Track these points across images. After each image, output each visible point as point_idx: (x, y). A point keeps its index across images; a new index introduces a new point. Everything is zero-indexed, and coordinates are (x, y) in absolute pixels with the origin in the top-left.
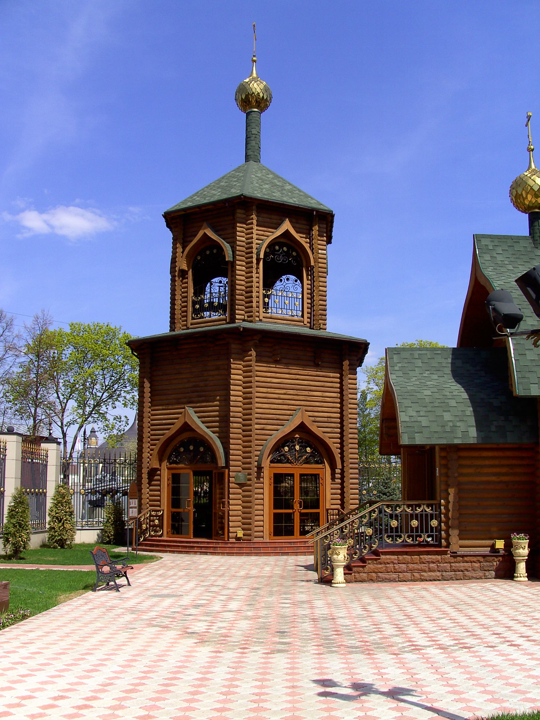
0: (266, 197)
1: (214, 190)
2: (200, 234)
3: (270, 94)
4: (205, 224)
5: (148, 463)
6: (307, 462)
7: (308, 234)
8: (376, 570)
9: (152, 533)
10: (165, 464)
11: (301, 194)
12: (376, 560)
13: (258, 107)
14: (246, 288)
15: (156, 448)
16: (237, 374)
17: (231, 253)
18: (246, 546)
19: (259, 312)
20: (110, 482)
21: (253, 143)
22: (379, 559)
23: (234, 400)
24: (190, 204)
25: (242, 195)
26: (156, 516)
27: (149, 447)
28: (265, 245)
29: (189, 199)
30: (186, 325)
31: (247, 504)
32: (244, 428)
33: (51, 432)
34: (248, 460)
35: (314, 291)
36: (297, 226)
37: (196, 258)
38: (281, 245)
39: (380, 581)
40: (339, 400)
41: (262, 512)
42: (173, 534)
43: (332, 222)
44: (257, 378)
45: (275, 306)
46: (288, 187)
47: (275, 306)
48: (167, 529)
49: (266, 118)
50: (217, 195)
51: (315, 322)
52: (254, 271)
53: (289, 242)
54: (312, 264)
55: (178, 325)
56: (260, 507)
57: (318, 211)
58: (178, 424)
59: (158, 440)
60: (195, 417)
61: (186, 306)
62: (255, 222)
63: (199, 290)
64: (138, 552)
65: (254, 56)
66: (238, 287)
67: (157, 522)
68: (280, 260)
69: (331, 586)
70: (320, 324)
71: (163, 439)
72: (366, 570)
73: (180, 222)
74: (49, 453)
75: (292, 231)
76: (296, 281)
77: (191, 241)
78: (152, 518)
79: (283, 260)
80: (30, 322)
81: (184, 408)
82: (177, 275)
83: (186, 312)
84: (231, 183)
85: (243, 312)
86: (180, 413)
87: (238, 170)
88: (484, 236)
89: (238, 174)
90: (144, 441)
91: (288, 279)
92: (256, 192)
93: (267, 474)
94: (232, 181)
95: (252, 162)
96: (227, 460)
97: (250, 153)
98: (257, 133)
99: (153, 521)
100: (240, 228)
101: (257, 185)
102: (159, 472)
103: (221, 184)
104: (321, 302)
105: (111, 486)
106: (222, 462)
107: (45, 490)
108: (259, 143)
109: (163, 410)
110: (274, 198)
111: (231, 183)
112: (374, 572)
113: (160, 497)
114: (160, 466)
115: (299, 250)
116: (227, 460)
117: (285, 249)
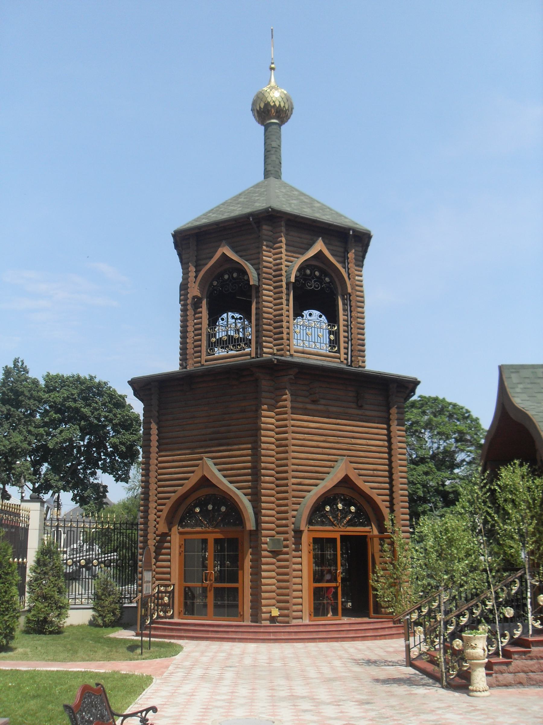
0: (296, 211)
1: (232, 206)
3: (291, 103)
4: (224, 242)
5: (155, 527)
6: (351, 523)
8: (525, 669)
9: (161, 614)
10: (175, 529)
11: (333, 212)
12: (525, 653)
13: (278, 117)
14: (275, 316)
15: (166, 509)
16: (268, 419)
17: (257, 276)
18: (279, 629)
19: (289, 346)
20: (87, 552)
21: (274, 157)
22: (530, 652)
23: (266, 447)
25: (270, 207)
26: (166, 592)
27: (156, 508)
28: (296, 267)
29: (204, 217)
30: (200, 362)
31: (283, 577)
32: (278, 482)
33: (24, 495)
34: (284, 522)
35: (351, 322)
36: (331, 248)
37: (211, 284)
39: (533, 685)
41: (299, 587)
42: (185, 614)
43: (367, 245)
44: (293, 422)
45: (308, 340)
47: (308, 340)
48: (179, 609)
49: (287, 130)
50: (237, 211)
51: (353, 359)
52: (284, 297)
53: (321, 265)
54: (349, 290)
55: (190, 362)
56: (298, 580)
57: (354, 230)
58: (194, 479)
59: (168, 498)
60: (215, 469)
61: (200, 340)
63: (213, 323)
64: (152, 639)
65: (272, 63)
66: (265, 315)
67: (166, 599)
68: (311, 286)
69: (469, 695)
70: (358, 361)
71: (174, 497)
72: (511, 668)
73: (192, 242)
74: (32, 515)
76: (320, 316)
77: (206, 264)
78: (160, 595)
79: (315, 287)
81: (201, 459)
82: (189, 305)
83: (200, 346)
84: (253, 198)
85: (271, 345)
86: (197, 466)
87: (257, 186)
89: (258, 190)
90: (150, 500)
91: (310, 315)
92: (284, 206)
93: (306, 539)
94: (253, 196)
96: (258, 522)
97: (269, 168)
98: (277, 146)
99: (162, 599)
101: (283, 199)
102: (169, 538)
103: (240, 200)
104: (360, 336)
105: (88, 557)
106: (250, 525)
107: (25, 560)
108: (279, 157)
109: (174, 461)
110: (305, 213)
111: (253, 198)
112: (524, 672)
113: (170, 568)
114: (170, 530)
115: (333, 275)
116: (258, 522)
117: (317, 273)
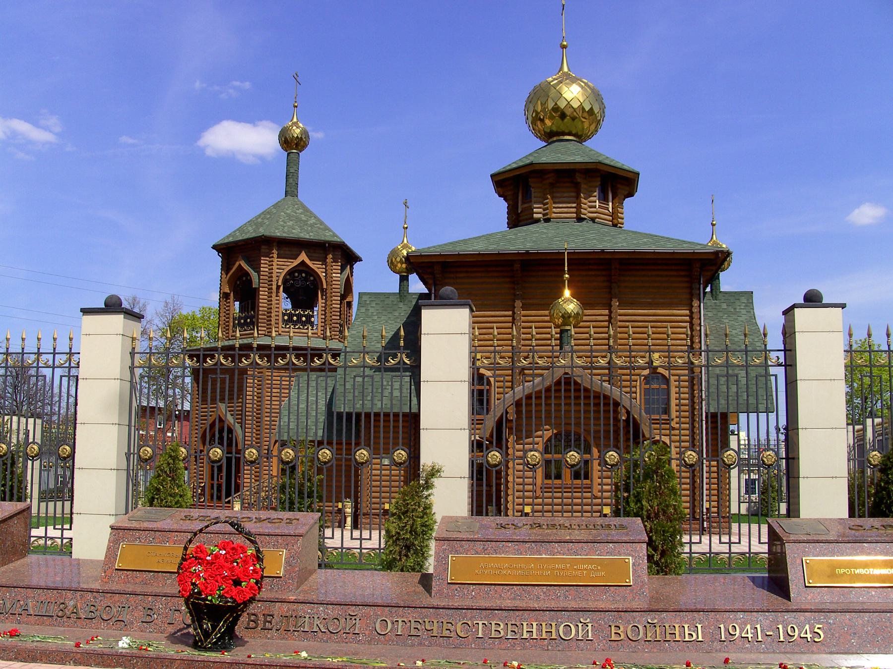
2: (237, 264)
7: (324, 261)
24: (231, 239)
28: (283, 275)
38: (300, 272)
40: (607, 318)
46: (312, 221)
50: (250, 234)
54: (325, 287)
62: (275, 256)
73: (228, 251)
75: (308, 261)
80: (160, 308)
88: (365, 294)
95: (289, 197)
100: (264, 261)
117: (304, 275)
